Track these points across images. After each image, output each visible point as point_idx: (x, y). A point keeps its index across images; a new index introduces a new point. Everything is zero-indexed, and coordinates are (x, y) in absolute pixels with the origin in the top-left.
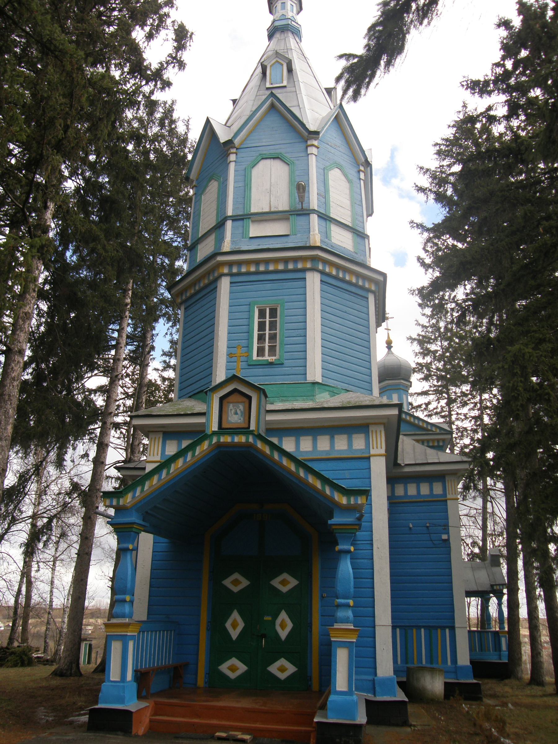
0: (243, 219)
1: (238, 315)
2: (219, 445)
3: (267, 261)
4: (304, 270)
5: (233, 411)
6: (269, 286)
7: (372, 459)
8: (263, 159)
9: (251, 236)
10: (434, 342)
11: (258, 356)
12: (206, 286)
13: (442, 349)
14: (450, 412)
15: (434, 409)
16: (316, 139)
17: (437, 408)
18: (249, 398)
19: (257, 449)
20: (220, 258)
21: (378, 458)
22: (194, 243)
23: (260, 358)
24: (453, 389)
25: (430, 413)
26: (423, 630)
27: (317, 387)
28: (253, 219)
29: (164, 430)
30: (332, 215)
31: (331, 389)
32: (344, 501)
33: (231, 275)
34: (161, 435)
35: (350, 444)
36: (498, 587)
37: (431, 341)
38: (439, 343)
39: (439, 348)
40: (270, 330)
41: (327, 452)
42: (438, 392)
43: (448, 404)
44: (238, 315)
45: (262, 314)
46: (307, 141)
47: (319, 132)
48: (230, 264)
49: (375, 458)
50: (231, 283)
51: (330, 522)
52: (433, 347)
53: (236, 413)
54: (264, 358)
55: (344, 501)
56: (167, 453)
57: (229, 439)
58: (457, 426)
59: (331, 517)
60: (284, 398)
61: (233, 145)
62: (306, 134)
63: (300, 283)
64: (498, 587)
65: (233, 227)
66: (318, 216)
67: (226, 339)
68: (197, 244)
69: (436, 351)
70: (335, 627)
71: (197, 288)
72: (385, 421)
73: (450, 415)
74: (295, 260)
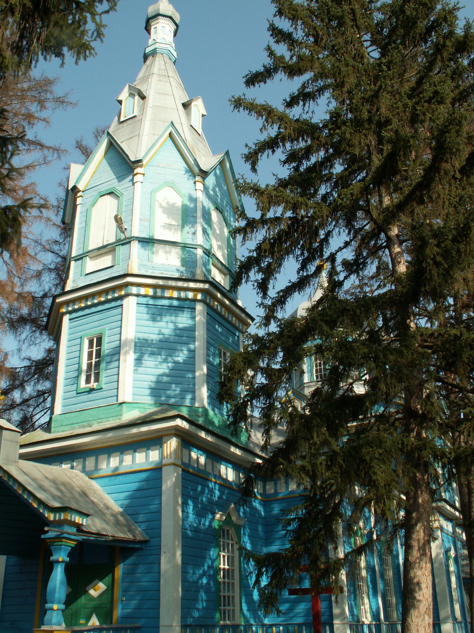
0: (82, 258)
1: (74, 349)
3: (93, 295)
4: (121, 298)
7: (164, 469)
8: (101, 196)
9: (87, 273)
16: (141, 167)
20: (129, 279)
21: (168, 467)
23: (87, 385)
26: (304, 628)
28: (91, 256)
30: (156, 237)
31: (141, 405)
33: (70, 312)
35: (147, 457)
41: (131, 466)
44: (74, 349)
45: (91, 345)
47: (141, 160)
48: (67, 303)
50: (70, 320)
56: (151, 460)
60: (100, 420)
63: (119, 310)
65: (75, 267)
66: (139, 241)
70: (42, 629)
72: (173, 432)
74: (113, 289)
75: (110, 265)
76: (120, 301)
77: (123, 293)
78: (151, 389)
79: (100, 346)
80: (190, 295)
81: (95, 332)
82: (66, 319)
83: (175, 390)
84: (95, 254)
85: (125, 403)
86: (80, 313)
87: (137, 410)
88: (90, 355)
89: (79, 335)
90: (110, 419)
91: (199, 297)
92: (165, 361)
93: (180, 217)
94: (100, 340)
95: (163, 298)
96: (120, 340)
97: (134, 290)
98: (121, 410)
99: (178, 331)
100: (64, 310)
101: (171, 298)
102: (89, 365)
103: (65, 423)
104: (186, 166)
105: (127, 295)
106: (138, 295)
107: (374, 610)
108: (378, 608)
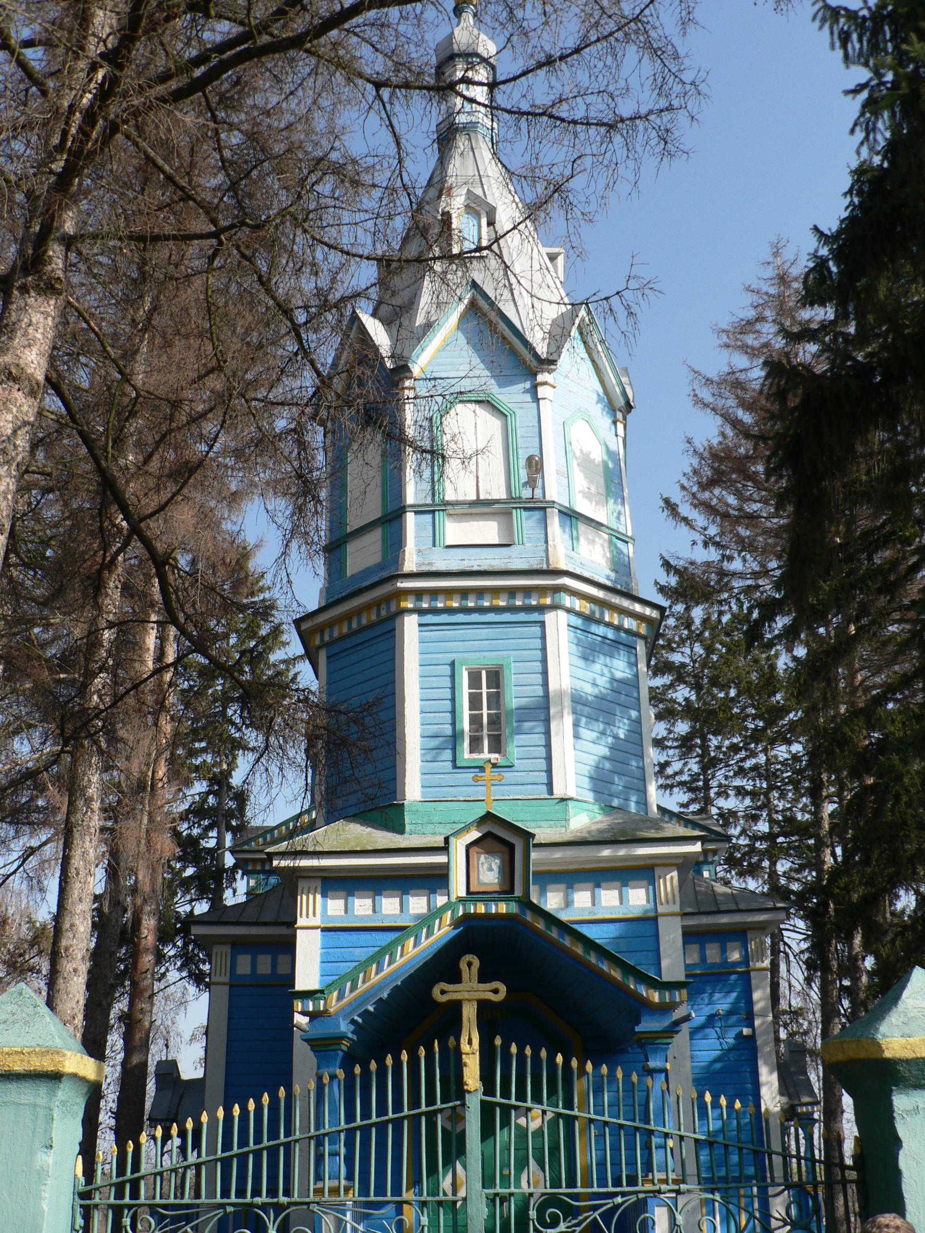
1: (435, 682)
2: (467, 917)
3: (480, 592)
4: (541, 609)
5: (486, 866)
6: (484, 632)
7: (660, 920)
9: (448, 543)
10: (678, 647)
11: (471, 752)
12: (371, 626)
13: (694, 662)
14: (706, 782)
15: (676, 774)
17: (681, 772)
18: (511, 847)
19: (526, 925)
21: (670, 918)
22: (338, 540)
24: (714, 741)
25: (669, 782)
27: (570, 803)
28: (451, 512)
29: (323, 874)
32: (656, 997)
33: (421, 612)
34: (319, 883)
36: (804, 1109)
37: (674, 645)
38: (688, 651)
39: (687, 661)
40: (489, 709)
42: (685, 744)
43: (704, 768)
44: (435, 682)
46: (536, 375)
48: (419, 594)
49: (665, 918)
51: (637, 1029)
52: (676, 658)
53: (490, 869)
54: (482, 756)
55: (656, 997)
57: (481, 909)
58: (719, 808)
59: (638, 1022)
61: (408, 374)
62: (534, 364)
64: (804, 1109)
67: (418, 724)
68: (346, 542)
69: (683, 665)
71: (355, 625)
72: (680, 861)
73: (707, 787)
74: (528, 591)
75: (497, 542)
76: (536, 614)
77: (548, 601)
78: (591, 778)
79: (498, 686)
80: (629, 623)
81: (489, 659)
82: (411, 623)
83: (619, 783)
84: (461, 511)
85: (571, 799)
86: (444, 618)
87: (585, 814)
88: (475, 702)
89: (450, 657)
90: (543, 824)
91: (643, 630)
92: (603, 733)
93: (601, 481)
94: (495, 677)
95: (600, 622)
96: (545, 684)
97: (567, 601)
98: (566, 811)
99: (615, 684)
100: (410, 605)
101: (609, 625)
102: (475, 720)
103: (436, 819)
104: (601, 390)
105: (555, 607)
106: (569, 611)
107: (506, 1130)
108: (501, 1128)
